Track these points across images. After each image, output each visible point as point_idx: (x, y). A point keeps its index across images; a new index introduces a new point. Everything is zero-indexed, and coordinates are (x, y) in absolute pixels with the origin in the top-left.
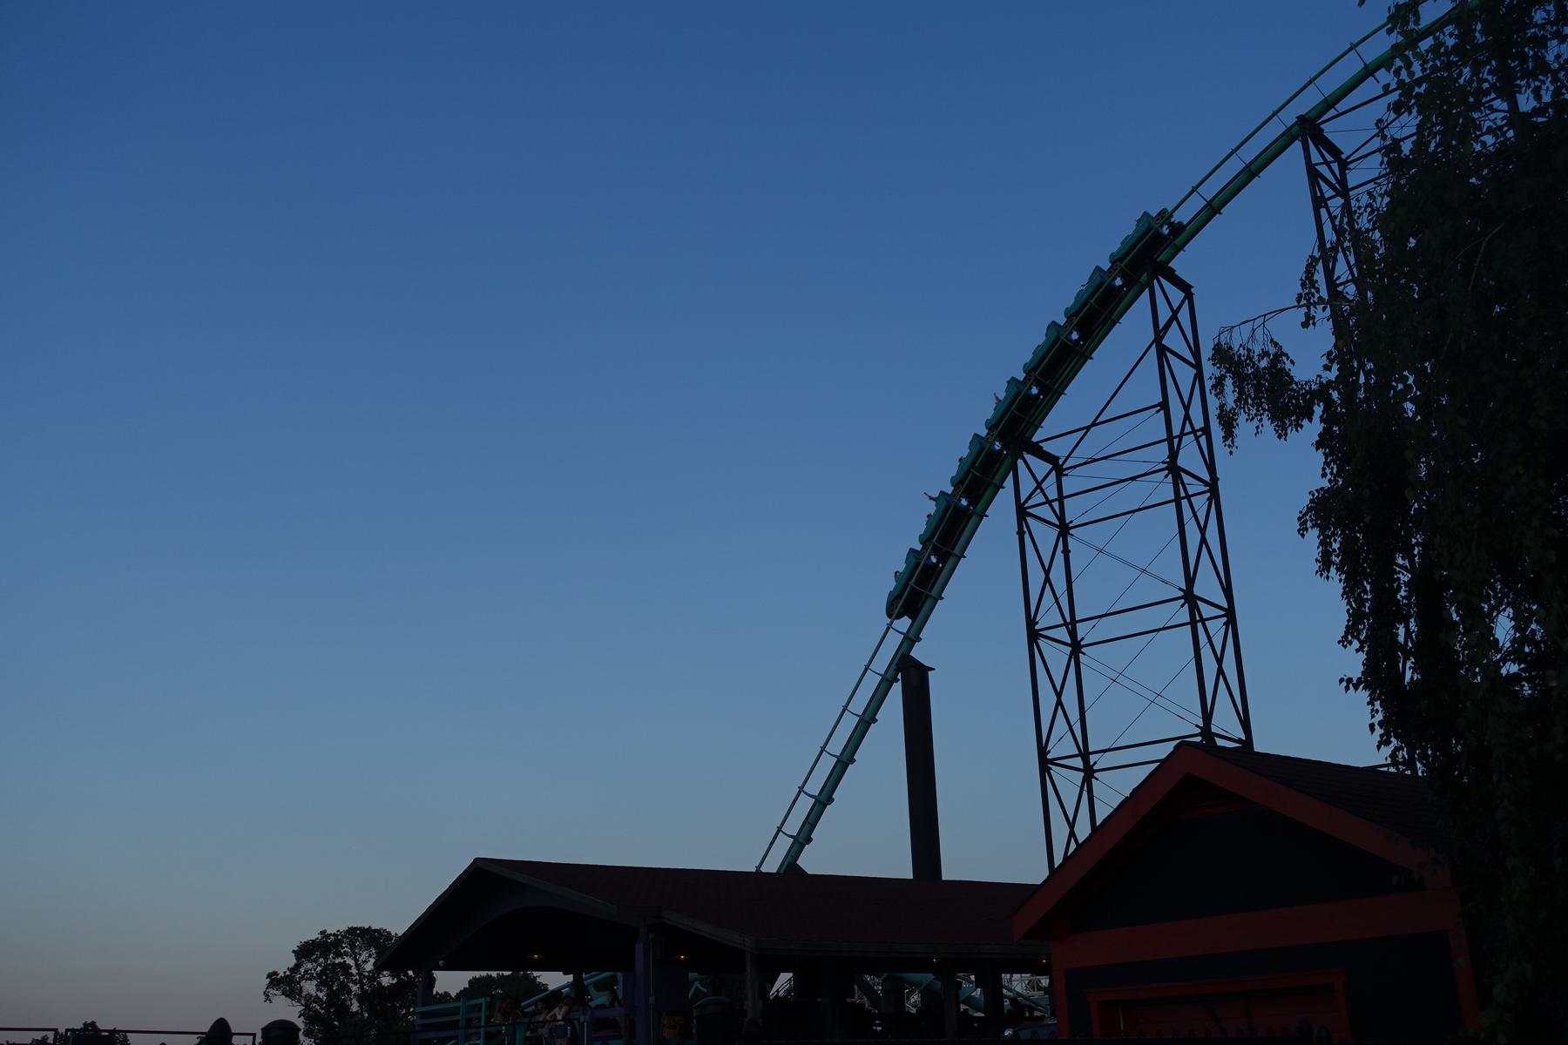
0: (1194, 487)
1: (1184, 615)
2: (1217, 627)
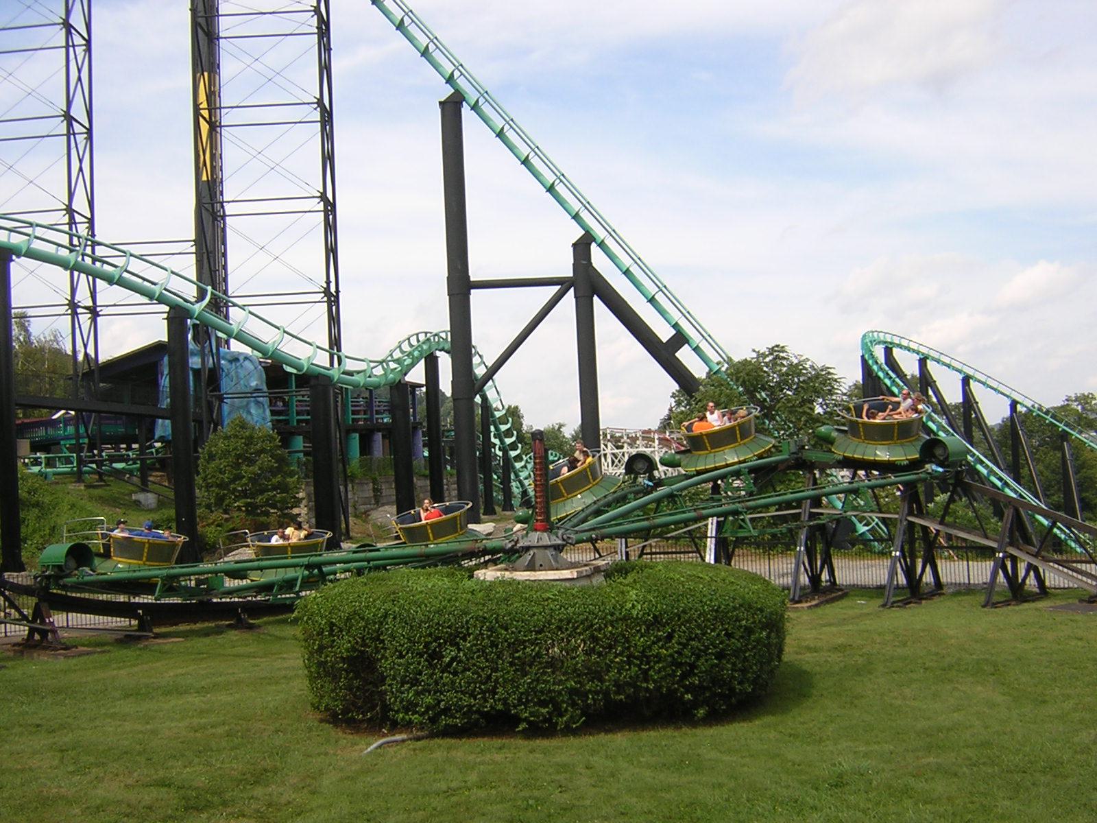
0: (78, 40)
1: (63, 129)
2: (81, 139)
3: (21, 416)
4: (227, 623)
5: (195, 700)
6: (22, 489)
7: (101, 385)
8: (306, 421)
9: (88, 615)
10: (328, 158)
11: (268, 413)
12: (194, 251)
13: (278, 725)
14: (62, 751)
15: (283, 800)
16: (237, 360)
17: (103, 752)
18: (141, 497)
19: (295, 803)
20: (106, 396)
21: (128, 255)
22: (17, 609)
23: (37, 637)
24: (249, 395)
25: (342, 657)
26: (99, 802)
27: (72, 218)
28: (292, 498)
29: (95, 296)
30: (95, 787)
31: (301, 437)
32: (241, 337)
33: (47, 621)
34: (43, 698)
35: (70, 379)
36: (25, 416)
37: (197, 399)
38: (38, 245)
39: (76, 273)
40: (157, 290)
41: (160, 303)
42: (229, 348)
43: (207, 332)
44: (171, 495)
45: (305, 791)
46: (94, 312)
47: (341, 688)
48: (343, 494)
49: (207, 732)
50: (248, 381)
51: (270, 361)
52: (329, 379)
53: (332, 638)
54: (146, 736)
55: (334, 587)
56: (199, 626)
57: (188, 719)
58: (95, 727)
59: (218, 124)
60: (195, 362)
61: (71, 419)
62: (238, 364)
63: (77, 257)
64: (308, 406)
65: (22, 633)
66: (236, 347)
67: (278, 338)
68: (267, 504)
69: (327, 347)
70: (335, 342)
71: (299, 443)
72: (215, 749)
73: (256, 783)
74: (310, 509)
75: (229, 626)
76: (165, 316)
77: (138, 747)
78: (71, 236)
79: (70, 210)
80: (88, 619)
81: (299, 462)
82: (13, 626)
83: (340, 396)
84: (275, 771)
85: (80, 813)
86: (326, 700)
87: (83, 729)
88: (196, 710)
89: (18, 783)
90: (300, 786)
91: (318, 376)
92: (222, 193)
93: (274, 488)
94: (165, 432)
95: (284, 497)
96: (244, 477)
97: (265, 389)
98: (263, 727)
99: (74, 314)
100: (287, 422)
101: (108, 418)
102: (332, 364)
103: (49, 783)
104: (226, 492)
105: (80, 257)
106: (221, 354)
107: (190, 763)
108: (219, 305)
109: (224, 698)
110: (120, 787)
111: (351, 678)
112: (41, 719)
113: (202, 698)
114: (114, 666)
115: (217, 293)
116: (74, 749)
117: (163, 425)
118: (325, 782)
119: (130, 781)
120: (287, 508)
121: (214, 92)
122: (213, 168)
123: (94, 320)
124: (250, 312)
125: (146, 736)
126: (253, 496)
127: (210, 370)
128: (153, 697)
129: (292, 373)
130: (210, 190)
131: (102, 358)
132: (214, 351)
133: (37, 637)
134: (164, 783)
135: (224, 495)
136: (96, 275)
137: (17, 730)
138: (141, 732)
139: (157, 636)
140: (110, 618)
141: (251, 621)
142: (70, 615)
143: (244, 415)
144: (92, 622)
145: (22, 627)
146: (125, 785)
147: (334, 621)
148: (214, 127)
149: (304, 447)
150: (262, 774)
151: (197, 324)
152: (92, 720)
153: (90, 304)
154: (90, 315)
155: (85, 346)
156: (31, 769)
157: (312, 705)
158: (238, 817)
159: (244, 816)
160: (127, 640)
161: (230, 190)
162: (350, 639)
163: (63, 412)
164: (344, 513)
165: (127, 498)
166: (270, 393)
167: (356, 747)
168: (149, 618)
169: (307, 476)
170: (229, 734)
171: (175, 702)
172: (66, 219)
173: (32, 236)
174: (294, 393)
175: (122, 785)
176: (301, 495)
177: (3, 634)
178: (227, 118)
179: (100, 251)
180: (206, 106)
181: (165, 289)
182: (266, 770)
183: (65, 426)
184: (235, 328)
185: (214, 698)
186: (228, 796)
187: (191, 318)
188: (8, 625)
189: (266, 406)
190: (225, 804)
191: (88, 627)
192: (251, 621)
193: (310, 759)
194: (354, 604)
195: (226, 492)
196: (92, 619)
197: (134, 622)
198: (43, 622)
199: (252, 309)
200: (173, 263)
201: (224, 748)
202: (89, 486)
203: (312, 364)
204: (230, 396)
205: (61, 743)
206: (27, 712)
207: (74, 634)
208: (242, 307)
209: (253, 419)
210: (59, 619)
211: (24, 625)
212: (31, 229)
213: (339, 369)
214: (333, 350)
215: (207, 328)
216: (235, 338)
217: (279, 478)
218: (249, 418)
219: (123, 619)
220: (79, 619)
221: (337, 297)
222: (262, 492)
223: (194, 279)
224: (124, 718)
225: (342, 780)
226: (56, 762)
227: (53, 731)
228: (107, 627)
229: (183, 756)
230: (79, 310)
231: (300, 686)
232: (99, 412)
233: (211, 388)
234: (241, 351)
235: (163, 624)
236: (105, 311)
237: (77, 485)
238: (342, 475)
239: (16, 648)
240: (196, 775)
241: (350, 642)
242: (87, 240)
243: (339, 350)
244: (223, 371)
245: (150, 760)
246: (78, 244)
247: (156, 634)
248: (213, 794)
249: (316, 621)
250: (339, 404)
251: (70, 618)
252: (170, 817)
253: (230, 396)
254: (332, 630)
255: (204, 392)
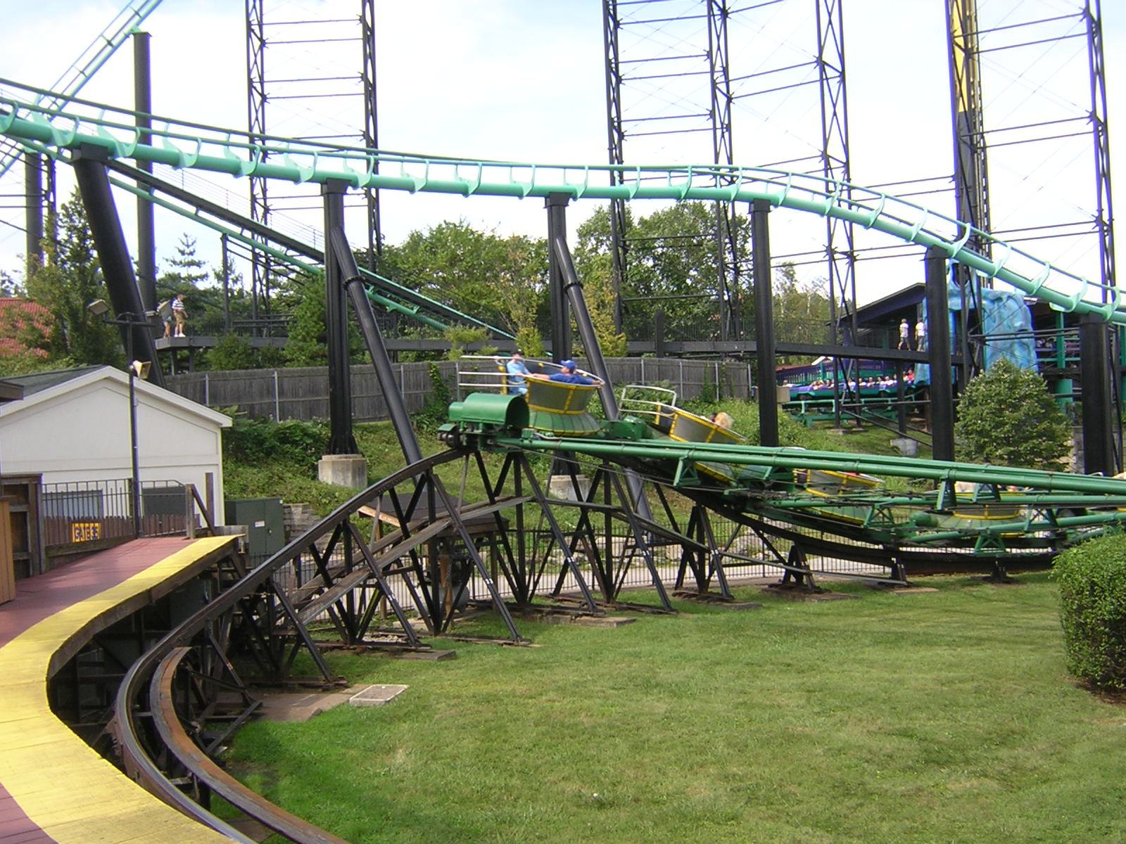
2: (834, 84)
3: (783, 362)
4: (984, 575)
5: (943, 653)
6: (782, 434)
7: (859, 330)
8: (1076, 363)
9: (843, 561)
10: (1098, 74)
11: (1033, 354)
12: (954, 187)
13: (1030, 686)
14: (808, 691)
15: (1029, 766)
16: (999, 299)
17: (848, 696)
18: (899, 443)
19: (1041, 769)
20: (867, 341)
21: (883, 196)
22: (775, 552)
23: (793, 579)
24: (1013, 336)
25: (1103, 619)
26: (841, 745)
27: (827, 163)
28: (1059, 446)
29: (852, 240)
30: (838, 730)
31: (1071, 380)
32: (1002, 276)
33: (803, 564)
34: (795, 639)
35: (829, 324)
36: (787, 363)
37: (958, 341)
38: (794, 195)
39: (833, 220)
40: (913, 231)
41: (917, 244)
42: (992, 287)
43: (967, 272)
44: (929, 441)
45: (1054, 758)
46: (851, 257)
47: (1101, 654)
48: (1117, 443)
49: (953, 686)
50: (1011, 320)
51: (1035, 299)
52: (1101, 316)
53: (1093, 599)
54: (892, 685)
55: (1098, 544)
56: (954, 577)
57: (935, 672)
58: (843, 671)
59: (975, 50)
60: (954, 303)
61: (829, 365)
62: (1001, 304)
63: (832, 203)
64: (1078, 346)
65: (779, 574)
66: (1000, 286)
67: (1043, 275)
68: (1032, 452)
69: (1100, 282)
70: (1109, 276)
71: (1068, 386)
72: (961, 705)
73: (1003, 743)
74: (1079, 458)
75: (985, 579)
76: (923, 257)
77: (883, 694)
78: (827, 183)
79: (825, 157)
80: (843, 564)
81: (1068, 408)
82: (771, 567)
83: (1114, 334)
84: (1023, 733)
85: (822, 754)
86: (1084, 665)
87: (831, 672)
88: (944, 664)
89: (767, 718)
90: (1049, 752)
91: (1089, 314)
92: (981, 123)
93: (1040, 435)
94: (924, 376)
95: (1051, 445)
96: (1007, 423)
97: (1030, 328)
98: (1014, 686)
99: (832, 259)
100: (1055, 364)
101: (865, 364)
102: (1105, 300)
103: (795, 721)
104: (986, 440)
105: (837, 202)
106: (983, 294)
107: (935, 716)
108: (978, 243)
109: (975, 653)
110: (862, 732)
111: (1113, 643)
112: (792, 659)
113: (952, 651)
114: (866, 612)
115: (979, 231)
116: (821, 690)
117: (922, 369)
118: (1077, 751)
119: (872, 728)
120: (1053, 457)
121: (970, 17)
122: (971, 98)
123: (852, 265)
124: (1012, 249)
125: (892, 685)
126: (1016, 444)
127: (971, 311)
128: (903, 647)
129: (1059, 312)
130: (967, 121)
131: (862, 302)
132: (975, 291)
133: (793, 579)
134: (905, 734)
135: (985, 442)
136: (852, 220)
137: (769, 667)
138: (888, 680)
139: (910, 585)
140: (864, 564)
141: (1010, 576)
142: (825, 559)
143: (1008, 358)
144: (847, 568)
145: (779, 569)
146: (868, 731)
147: (1096, 580)
148: (970, 54)
149: (1074, 391)
150: (1008, 735)
151: (957, 264)
152: (841, 664)
153: (847, 249)
154: (847, 260)
155: (843, 292)
156: (779, 706)
157: (1069, 668)
158: (979, 777)
159: (986, 776)
160: (881, 586)
161: (991, 119)
162: (1114, 600)
163: (822, 358)
164: (1118, 464)
165: (885, 444)
166: (1036, 334)
167: (1114, 718)
168: (903, 567)
169: (1076, 423)
170: (977, 691)
171: (924, 653)
172: (822, 165)
173: (789, 186)
174: (1063, 333)
175: (865, 730)
176: (1070, 443)
177: (762, 575)
178: (984, 42)
179: (856, 195)
180: (961, 33)
181: (922, 229)
182: (1013, 732)
183: (824, 372)
184: (996, 264)
185: (964, 653)
186: (971, 754)
187: (949, 257)
188: (766, 566)
189: (1031, 348)
190: (967, 761)
191: (843, 572)
192: (1010, 576)
193: (1061, 726)
194: (1119, 563)
195: (986, 440)
196: (838, 563)
197: (888, 570)
198: (799, 566)
199: (1016, 245)
200: (927, 202)
201: (971, 705)
202: (848, 431)
203: (1082, 301)
204: (992, 338)
205: (809, 684)
206: (779, 651)
207: (829, 578)
208: (1004, 244)
209: (1017, 361)
210: (814, 562)
211: (781, 567)
212: (787, 178)
213: (1113, 305)
214: (1107, 284)
215: (968, 268)
216: (996, 276)
217: (1045, 425)
218: (1013, 360)
219: (877, 566)
220: (834, 564)
221: (1111, 226)
222: (1026, 440)
223: (954, 217)
224: (872, 664)
225: (1096, 751)
226: (803, 702)
227: (803, 672)
228: (861, 573)
229: (928, 708)
230: (836, 256)
231: (1057, 652)
232: (857, 357)
233: (972, 330)
234: (1004, 290)
235: (917, 574)
236: (1089, 227)
237: (836, 430)
238: (1115, 422)
239: (773, 589)
240: (940, 728)
241: (1113, 604)
242: (843, 185)
243: (1113, 284)
244: (985, 311)
245: (895, 709)
246: (833, 189)
247: (908, 582)
248: (956, 750)
249: (1076, 580)
250: (1114, 343)
251: (825, 562)
252: (910, 768)
253: (992, 338)
254: (1093, 590)
255: (963, 334)
